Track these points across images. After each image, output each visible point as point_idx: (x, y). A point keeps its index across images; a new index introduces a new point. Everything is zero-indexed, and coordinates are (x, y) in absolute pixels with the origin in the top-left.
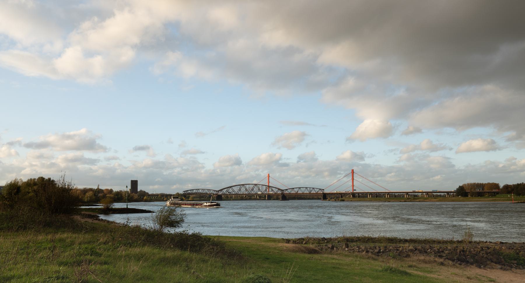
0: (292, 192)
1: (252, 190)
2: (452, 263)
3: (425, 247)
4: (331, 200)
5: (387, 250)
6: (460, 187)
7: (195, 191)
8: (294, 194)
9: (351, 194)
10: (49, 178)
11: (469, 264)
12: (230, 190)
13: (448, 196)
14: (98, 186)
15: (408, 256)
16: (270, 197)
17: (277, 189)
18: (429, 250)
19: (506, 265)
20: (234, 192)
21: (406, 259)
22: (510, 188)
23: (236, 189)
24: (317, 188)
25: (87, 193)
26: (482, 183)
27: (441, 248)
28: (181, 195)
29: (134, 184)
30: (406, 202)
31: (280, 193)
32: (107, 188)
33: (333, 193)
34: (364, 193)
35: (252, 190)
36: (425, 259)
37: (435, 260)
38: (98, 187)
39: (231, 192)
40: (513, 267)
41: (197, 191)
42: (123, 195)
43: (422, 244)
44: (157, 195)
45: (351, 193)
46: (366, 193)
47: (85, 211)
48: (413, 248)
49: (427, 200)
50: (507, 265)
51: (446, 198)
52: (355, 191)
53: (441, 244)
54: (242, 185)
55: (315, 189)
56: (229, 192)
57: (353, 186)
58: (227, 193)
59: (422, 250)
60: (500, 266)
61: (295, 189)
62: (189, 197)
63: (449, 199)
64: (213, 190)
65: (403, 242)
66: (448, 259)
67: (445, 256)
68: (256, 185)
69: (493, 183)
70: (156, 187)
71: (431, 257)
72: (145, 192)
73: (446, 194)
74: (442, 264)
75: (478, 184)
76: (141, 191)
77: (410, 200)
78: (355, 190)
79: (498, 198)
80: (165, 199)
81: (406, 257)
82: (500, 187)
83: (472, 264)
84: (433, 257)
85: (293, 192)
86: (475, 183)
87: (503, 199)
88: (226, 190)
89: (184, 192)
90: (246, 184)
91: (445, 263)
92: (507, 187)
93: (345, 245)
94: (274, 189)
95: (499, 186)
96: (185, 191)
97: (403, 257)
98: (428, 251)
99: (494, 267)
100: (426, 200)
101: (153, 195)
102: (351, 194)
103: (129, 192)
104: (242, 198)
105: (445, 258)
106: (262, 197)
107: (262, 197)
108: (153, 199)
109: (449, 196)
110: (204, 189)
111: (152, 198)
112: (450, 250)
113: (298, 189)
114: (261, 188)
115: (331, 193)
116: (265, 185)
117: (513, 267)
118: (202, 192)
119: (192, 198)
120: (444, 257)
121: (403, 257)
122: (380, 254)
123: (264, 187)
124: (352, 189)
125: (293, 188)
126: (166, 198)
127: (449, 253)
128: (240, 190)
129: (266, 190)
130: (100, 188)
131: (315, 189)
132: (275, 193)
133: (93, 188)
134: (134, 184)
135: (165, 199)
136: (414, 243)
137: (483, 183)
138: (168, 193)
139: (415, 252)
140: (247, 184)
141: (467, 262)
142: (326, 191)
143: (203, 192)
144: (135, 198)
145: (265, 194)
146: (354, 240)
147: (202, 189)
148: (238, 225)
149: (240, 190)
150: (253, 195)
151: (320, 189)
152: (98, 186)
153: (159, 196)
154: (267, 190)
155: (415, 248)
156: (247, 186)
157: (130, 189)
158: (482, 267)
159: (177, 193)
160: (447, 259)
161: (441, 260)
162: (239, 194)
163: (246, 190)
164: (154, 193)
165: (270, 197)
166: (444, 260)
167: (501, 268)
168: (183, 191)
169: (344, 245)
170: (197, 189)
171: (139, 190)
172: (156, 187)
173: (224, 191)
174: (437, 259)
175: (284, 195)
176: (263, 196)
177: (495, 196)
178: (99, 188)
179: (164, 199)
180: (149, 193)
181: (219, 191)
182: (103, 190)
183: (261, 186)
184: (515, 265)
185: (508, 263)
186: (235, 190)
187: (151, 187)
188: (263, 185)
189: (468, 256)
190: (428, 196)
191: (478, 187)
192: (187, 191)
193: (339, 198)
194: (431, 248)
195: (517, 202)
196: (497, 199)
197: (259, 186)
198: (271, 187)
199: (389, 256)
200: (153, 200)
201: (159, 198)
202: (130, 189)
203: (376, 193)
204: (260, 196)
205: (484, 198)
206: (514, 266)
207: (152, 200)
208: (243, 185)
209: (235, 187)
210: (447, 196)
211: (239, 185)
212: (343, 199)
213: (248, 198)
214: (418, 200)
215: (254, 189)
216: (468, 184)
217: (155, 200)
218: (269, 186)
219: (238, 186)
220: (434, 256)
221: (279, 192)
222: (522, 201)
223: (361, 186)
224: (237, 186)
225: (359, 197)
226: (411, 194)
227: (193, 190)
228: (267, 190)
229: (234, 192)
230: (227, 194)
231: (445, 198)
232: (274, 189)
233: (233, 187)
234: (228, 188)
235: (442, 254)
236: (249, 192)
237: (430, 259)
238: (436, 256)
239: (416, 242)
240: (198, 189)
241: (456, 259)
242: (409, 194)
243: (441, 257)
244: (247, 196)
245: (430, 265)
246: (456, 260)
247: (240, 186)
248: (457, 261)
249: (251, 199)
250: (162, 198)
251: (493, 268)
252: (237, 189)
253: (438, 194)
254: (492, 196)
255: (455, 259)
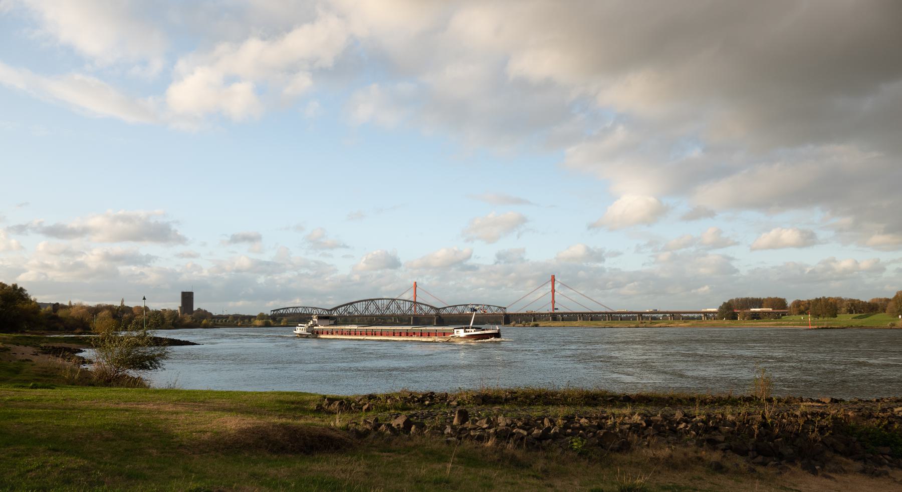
0: (453, 313)
1: (388, 308)
2: (745, 466)
3: (672, 415)
4: (516, 325)
5: (569, 431)
6: (725, 303)
7: (291, 310)
8: (456, 314)
9: (551, 316)
10: (13, 285)
11: (783, 462)
12: (351, 309)
13: (706, 319)
14: (123, 301)
15: (625, 447)
16: (418, 320)
17: (429, 308)
18: (682, 426)
19: (869, 458)
20: (356, 312)
21: (619, 456)
22: (803, 305)
23: (361, 307)
24: (495, 306)
25: (100, 313)
26: (759, 298)
27: (709, 416)
28: (268, 317)
29: (187, 298)
30: (638, 327)
31: (434, 313)
32: (139, 305)
33: (520, 314)
34: (571, 314)
35: (388, 308)
36: (671, 456)
37: (699, 455)
38: (122, 304)
39: (352, 313)
40: (885, 464)
41: (285, 310)
42: (165, 317)
43: (665, 406)
44: (227, 317)
45: (551, 313)
46: (574, 313)
47: (65, 342)
48: (642, 419)
49: (672, 325)
50: (871, 458)
51: (703, 321)
52: (556, 311)
53: (707, 407)
54: (370, 300)
55: (492, 307)
56: (349, 313)
57: (553, 302)
58: (346, 313)
59: (663, 426)
60: (859, 465)
61: (458, 307)
62: (280, 321)
63: (707, 323)
64: (321, 309)
65: (620, 401)
66: (730, 448)
67: (723, 442)
68: (394, 300)
69: (776, 298)
70: (240, 303)
71: (687, 446)
72: (205, 311)
73: (702, 315)
74: (718, 468)
75: (753, 299)
76: (199, 310)
77: (644, 325)
78: (557, 309)
79: (784, 321)
80: (239, 324)
81: (619, 450)
82: (787, 304)
83: (792, 461)
84: (694, 448)
85: (455, 312)
86: (749, 298)
87: (793, 323)
88: (343, 308)
89: (272, 312)
90: (376, 299)
91: (728, 464)
92: (798, 304)
93: (459, 416)
94: (424, 307)
95: (785, 302)
96: (274, 311)
97: (612, 450)
98: (679, 428)
99: (846, 468)
100: (670, 325)
101: (220, 317)
102: (551, 316)
103: (179, 312)
104: (371, 321)
105: (723, 446)
106: (402, 320)
107: (402, 320)
108: (218, 323)
109: (707, 319)
110: (307, 307)
111: (218, 322)
112: (733, 424)
113: (463, 307)
114: (401, 306)
115: (517, 314)
116: (410, 300)
117: (885, 464)
118: (303, 312)
119: (286, 322)
120: (720, 442)
121: (612, 450)
122: (545, 443)
123: (408, 305)
124: (552, 308)
125: (456, 306)
126: (242, 322)
127: (732, 433)
128: (368, 308)
129: (410, 309)
130: (126, 304)
131: (492, 307)
132: (426, 314)
133: (115, 305)
134: (187, 298)
135: (239, 324)
136: (647, 405)
137: (760, 299)
138: (246, 314)
139: (646, 433)
140: (378, 299)
141: (781, 457)
142: (509, 311)
143: (305, 312)
144: (187, 322)
145: (409, 315)
146: (502, 398)
147: (304, 307)
148: (368, 364)
149: (367, 308)
150: (390, 317)
151: (500, 307)
152: (123, 301)
153: (230, 319)
154: (413, 309)
155: (645, 422)
156: (379, 303)
157: (180, 307)
158: (817, 467)
159: (261, 313)
160: (730, 451)
161: (716, 456)
162: (366, 316)
163: (378, 308)
164: (225, 313)
165: (418, 320)
166: (724, 456)
167: (863, 472)
168: (271, 311)
169: (457, 415)
170: (294, 307)
171: (195, 309)
172: (240, 303)
173: (341, 310)
174: (704, 452)
175: (440, 316)
176: (407, 319)
177: (779, 318)
178: (124, 305)
179: (237, 323)
180: (214, 314)
181: (331, 310)
182: (132, 308)
183: (402, 302)
184: (887, 459)
185: (872, 453)
186: (359, 309)
187: (231, 304)
188: (406, 301)
189: (780, 437)
190: (674, 318)
191: (753, 303)
192: (278, 310)
193: (531, 321)
194: (687, 418)
195: (815, 327)
196: (783, 323)
197: (399, 303)
198: (418, 303)
199: (571, 448)
200: (219, 325)
201: (229, 322)
202: (180, 306)
203: (591, 313)
204: (401, 318)
205: (762, 322)
206: (887, 462)
207: (216, 325)
208: (372, 300)
209: (359, 303)
210: (703, 319)
211: (365, 301)
212: (536, 323)
213: (380, 322)
214: (657, 325)
215: (391, 307)
216: (737, 300)
217: (221, 325)
218: (415, 302)
219: (364, 303)
220: (697, 444)
221: (433, 312)
222: (825, 326)
223: (568, 301)
224: (361, 303)
225: (563, 320)
226: (646, 316)
227: (288, 308)
228: (413, 309)
229: (356, 312)
230: (345, 316)
231: (700, 322)
232: (424, 307)
233: (356, 304)
234: (347, 305)
235: (715, 435)
236: (383, 312)
237: (685, 454)
238: (700, 444)
239: (650, 401)
240: (297, 307)
241: (751, 448)
242: (643, 315)
243: (713, 444)
244: (380, 318)
245: (686, 473)
246: (753, 450)
247: (367, 303)
248: (755, 453)
249: (386, 323)
250: (235, 322)
251: (845, 472)
252: (361, 306)
253: (690, 315)
254: (775, 319)
255: (749, 450)
